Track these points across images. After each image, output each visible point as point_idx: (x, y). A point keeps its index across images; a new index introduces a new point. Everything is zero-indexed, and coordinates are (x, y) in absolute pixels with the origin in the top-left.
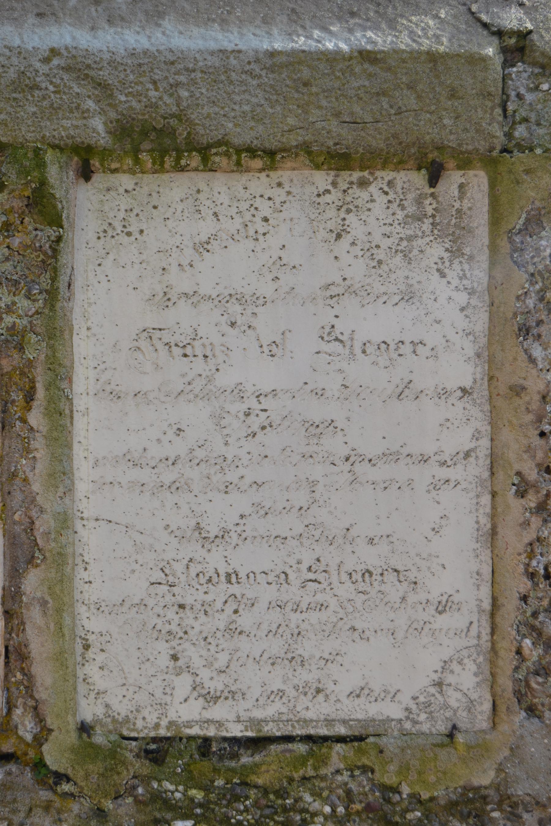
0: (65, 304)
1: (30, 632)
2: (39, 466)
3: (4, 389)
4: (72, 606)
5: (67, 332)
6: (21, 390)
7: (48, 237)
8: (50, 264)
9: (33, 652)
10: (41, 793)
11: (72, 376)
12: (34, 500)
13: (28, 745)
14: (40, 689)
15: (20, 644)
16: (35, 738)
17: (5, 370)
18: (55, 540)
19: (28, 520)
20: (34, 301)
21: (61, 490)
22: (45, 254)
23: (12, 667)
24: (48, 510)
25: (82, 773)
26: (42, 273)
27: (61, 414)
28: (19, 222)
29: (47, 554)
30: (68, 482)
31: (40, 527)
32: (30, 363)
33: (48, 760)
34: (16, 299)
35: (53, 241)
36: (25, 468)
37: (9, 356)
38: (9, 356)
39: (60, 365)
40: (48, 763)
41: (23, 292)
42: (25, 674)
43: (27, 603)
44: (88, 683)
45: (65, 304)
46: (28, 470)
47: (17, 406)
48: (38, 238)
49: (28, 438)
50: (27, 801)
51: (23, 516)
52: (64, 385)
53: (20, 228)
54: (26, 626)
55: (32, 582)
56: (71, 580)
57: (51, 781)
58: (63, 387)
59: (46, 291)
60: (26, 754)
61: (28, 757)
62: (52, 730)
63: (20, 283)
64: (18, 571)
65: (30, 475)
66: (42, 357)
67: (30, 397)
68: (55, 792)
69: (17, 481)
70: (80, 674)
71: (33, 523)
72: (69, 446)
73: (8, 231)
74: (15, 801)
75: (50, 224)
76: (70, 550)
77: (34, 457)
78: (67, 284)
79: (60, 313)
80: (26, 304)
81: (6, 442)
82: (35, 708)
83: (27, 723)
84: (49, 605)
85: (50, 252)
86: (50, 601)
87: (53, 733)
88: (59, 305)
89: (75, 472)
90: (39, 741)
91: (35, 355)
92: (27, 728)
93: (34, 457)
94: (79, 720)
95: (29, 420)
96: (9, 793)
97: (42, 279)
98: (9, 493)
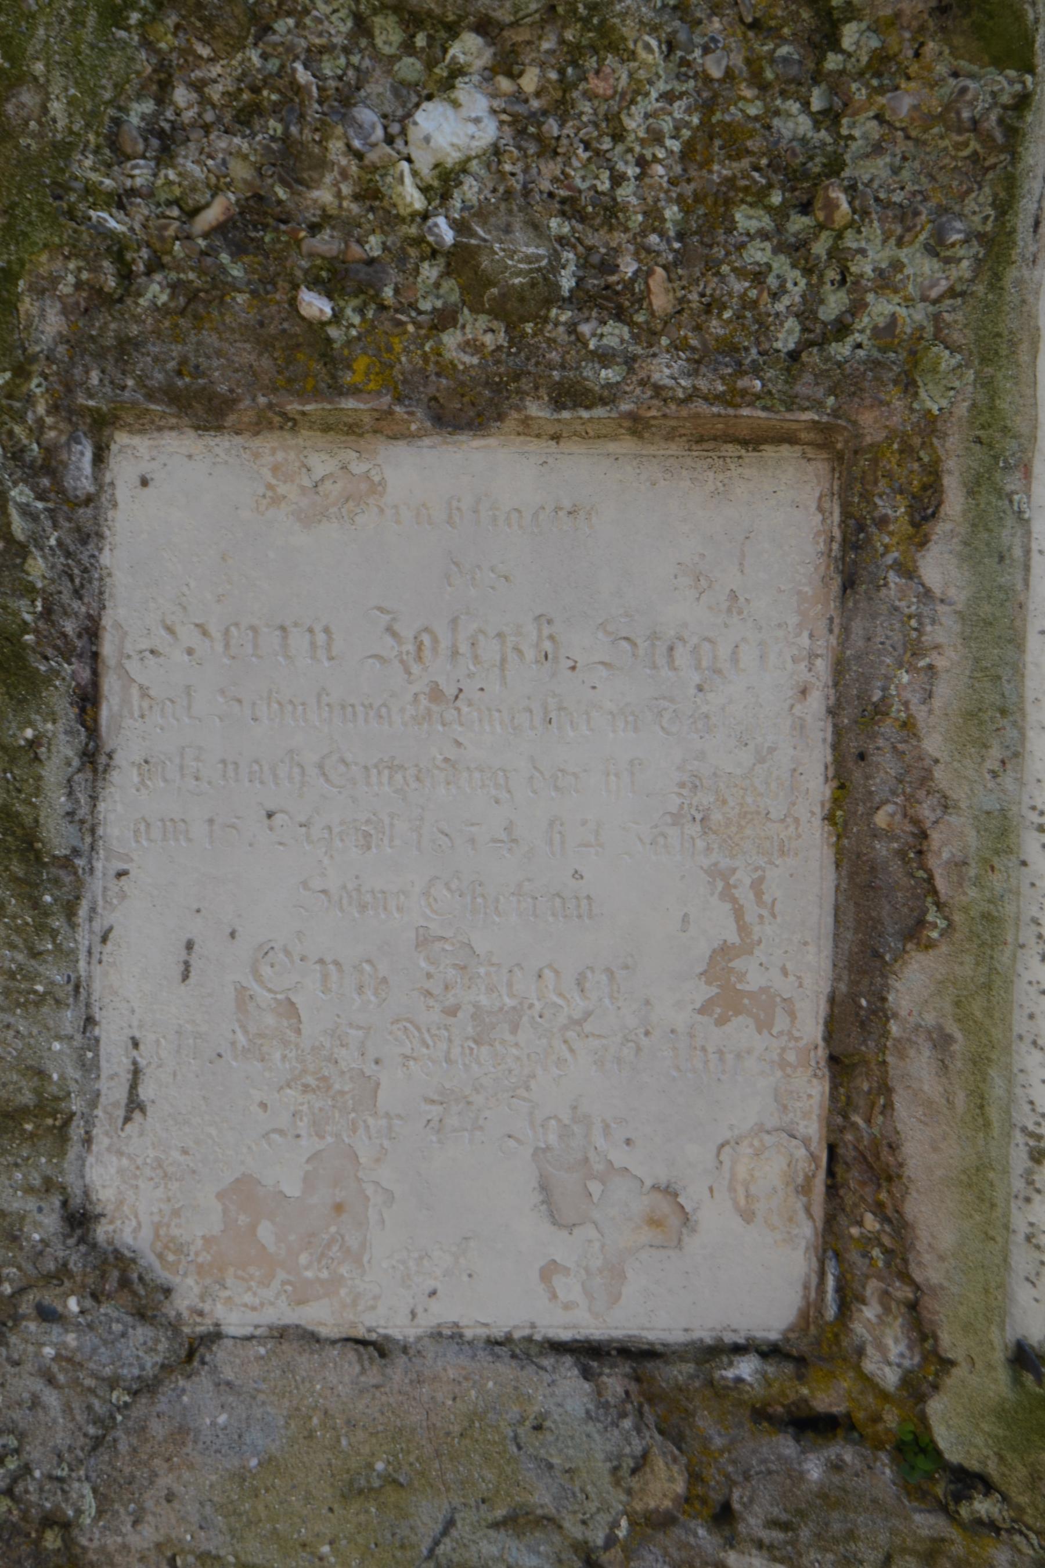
0: (1026, 273)
1: (906, 1115)
2: (943, 690)
3: (858, 487)
4: (1007, 1050)
5: (1024, 346)
6: (901, 492)
7: (994, 94)
8: (993, 167)
9: (911, 1163)
10: (918, 1518)
11: (1030, 460)
12: (926, 778)
13: (884, 1396)
14: (926, 1258)
15: (875, 1143)
16: (908, 1381)
17: (868, 440)
18: (978, 882)
19: (909, 828)
20: (947, 261)
21: (996, 752)
22: (987, 139)
23: (849, 1200)
24: (963, 805)
25: (1022, 1472)
26: (970, 191)
27: (1001, 559)
28: (910, 53)
29: (957, 917)
30: (1012, 733)
31: (943, 849)
32: (931, 425)
33: (943, 1437)
34: (903, 254)
35: (1005, 107)
36: (907, 695)
37: (882, 403)
38: (882, 403)
39: (1005, 430)
40: (942, 1445)
41: (922, 237)
42: (886, 1219)
43: (898, 1040)
44: (1038, 1247)
45: (1026, 273)
46: (914, 700)
47: (891, 534)
48: (969, 97)
49: (919, 616)
50: (883, 1538)
51: (898, 817)
52: (1012, 483)
53: (914, 69)
54: (896, 1098)
55: (915, 987)
56: (1008, 984)
57: (939, 1490)
58: (1009, 488)
59: (980, 236)
60: (876, 1419)
61: (880, 1427)
62: (952, 1363)
63: (917, 213)
64: (881, 957)
65: (920, 712)
66: (962, 409)
67: (924, 510)
68: (953, 1518)
69: (887, 728)
70: (1019, 1223)
71: (924, 835)
72: (1017, 641)
73: (878, 75)
74: (851, 1535)
75: (999, 63)
76: (1010, 909)
77: (931, 667)
78: (1031, 221)
79: (1012, 295)
80: (926, 269)
81: (857, 627)
82: (913, 1306)
83: (890, 1342)
84: (955, 1047)
85: (999, 136)
86: (958, 1035)
87: (955, 1371)
88: (1011, 274)
89: (1029, 708)
90: (916, 1389)
91: (944, 403)
92: (887, 1356)
93: (931, 667)
94: (1011, 1337)
95: (922, 571)
96: (835, 1515)
97: (970, 204)
98: (862, 756)
